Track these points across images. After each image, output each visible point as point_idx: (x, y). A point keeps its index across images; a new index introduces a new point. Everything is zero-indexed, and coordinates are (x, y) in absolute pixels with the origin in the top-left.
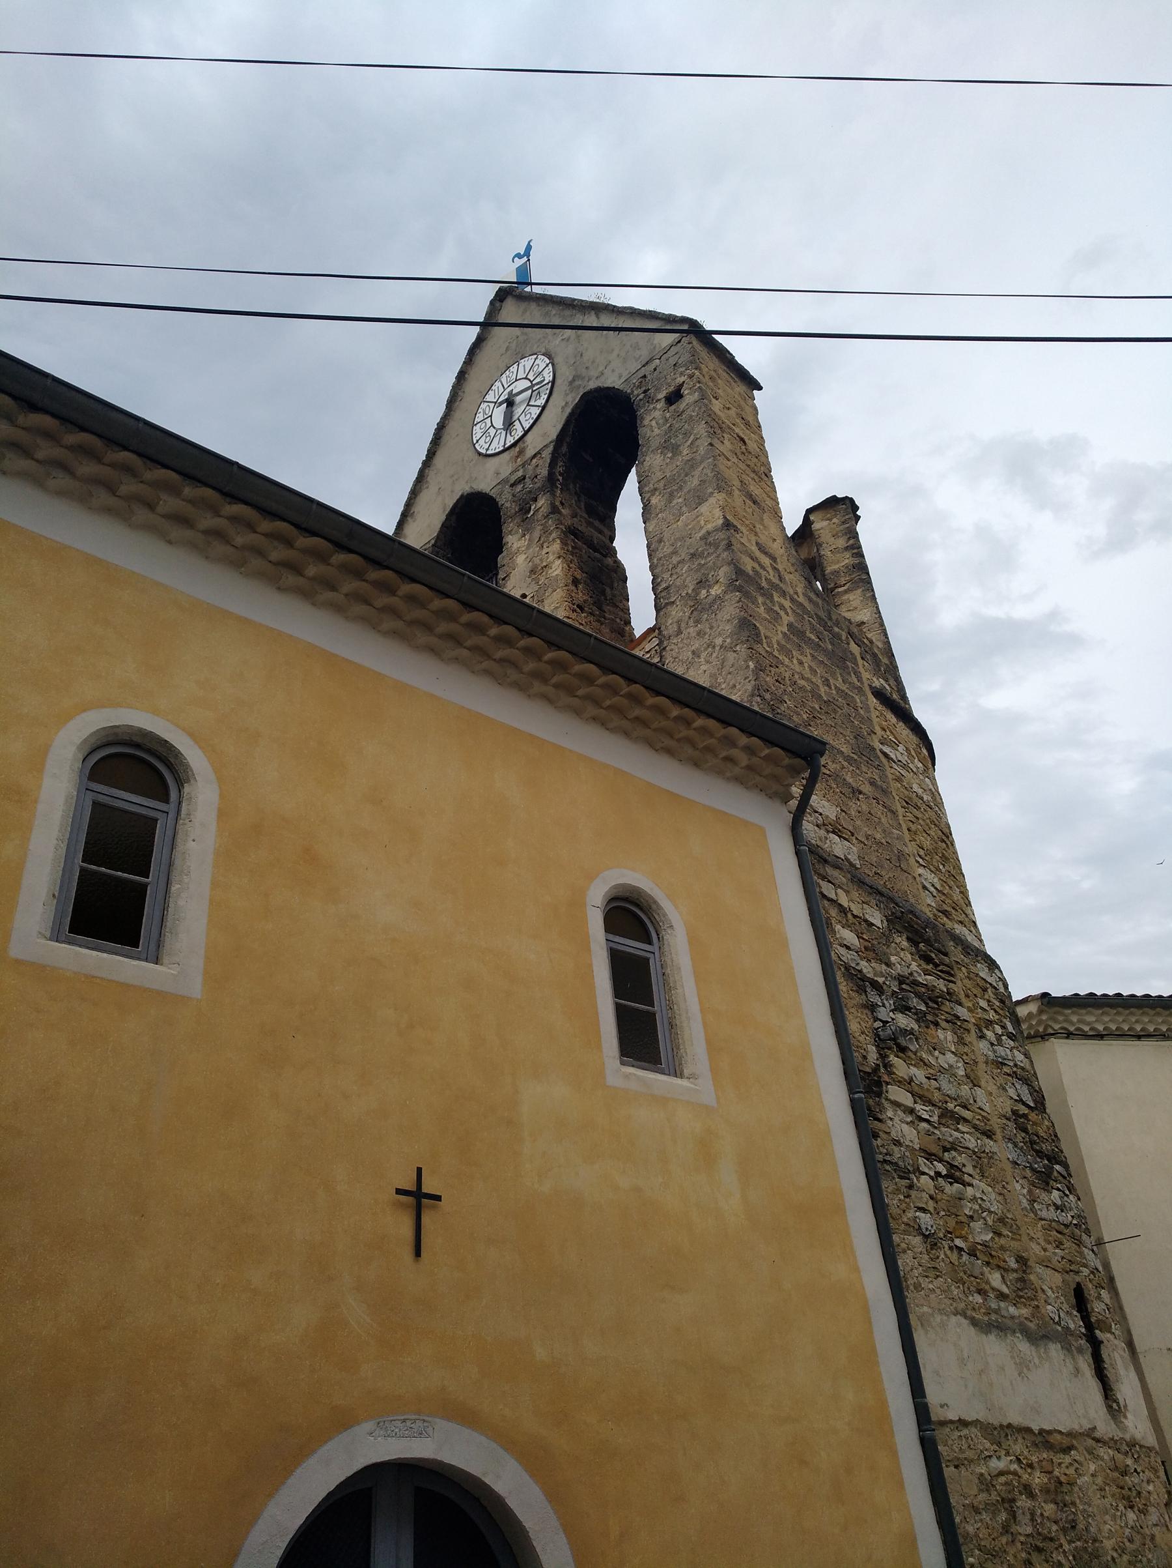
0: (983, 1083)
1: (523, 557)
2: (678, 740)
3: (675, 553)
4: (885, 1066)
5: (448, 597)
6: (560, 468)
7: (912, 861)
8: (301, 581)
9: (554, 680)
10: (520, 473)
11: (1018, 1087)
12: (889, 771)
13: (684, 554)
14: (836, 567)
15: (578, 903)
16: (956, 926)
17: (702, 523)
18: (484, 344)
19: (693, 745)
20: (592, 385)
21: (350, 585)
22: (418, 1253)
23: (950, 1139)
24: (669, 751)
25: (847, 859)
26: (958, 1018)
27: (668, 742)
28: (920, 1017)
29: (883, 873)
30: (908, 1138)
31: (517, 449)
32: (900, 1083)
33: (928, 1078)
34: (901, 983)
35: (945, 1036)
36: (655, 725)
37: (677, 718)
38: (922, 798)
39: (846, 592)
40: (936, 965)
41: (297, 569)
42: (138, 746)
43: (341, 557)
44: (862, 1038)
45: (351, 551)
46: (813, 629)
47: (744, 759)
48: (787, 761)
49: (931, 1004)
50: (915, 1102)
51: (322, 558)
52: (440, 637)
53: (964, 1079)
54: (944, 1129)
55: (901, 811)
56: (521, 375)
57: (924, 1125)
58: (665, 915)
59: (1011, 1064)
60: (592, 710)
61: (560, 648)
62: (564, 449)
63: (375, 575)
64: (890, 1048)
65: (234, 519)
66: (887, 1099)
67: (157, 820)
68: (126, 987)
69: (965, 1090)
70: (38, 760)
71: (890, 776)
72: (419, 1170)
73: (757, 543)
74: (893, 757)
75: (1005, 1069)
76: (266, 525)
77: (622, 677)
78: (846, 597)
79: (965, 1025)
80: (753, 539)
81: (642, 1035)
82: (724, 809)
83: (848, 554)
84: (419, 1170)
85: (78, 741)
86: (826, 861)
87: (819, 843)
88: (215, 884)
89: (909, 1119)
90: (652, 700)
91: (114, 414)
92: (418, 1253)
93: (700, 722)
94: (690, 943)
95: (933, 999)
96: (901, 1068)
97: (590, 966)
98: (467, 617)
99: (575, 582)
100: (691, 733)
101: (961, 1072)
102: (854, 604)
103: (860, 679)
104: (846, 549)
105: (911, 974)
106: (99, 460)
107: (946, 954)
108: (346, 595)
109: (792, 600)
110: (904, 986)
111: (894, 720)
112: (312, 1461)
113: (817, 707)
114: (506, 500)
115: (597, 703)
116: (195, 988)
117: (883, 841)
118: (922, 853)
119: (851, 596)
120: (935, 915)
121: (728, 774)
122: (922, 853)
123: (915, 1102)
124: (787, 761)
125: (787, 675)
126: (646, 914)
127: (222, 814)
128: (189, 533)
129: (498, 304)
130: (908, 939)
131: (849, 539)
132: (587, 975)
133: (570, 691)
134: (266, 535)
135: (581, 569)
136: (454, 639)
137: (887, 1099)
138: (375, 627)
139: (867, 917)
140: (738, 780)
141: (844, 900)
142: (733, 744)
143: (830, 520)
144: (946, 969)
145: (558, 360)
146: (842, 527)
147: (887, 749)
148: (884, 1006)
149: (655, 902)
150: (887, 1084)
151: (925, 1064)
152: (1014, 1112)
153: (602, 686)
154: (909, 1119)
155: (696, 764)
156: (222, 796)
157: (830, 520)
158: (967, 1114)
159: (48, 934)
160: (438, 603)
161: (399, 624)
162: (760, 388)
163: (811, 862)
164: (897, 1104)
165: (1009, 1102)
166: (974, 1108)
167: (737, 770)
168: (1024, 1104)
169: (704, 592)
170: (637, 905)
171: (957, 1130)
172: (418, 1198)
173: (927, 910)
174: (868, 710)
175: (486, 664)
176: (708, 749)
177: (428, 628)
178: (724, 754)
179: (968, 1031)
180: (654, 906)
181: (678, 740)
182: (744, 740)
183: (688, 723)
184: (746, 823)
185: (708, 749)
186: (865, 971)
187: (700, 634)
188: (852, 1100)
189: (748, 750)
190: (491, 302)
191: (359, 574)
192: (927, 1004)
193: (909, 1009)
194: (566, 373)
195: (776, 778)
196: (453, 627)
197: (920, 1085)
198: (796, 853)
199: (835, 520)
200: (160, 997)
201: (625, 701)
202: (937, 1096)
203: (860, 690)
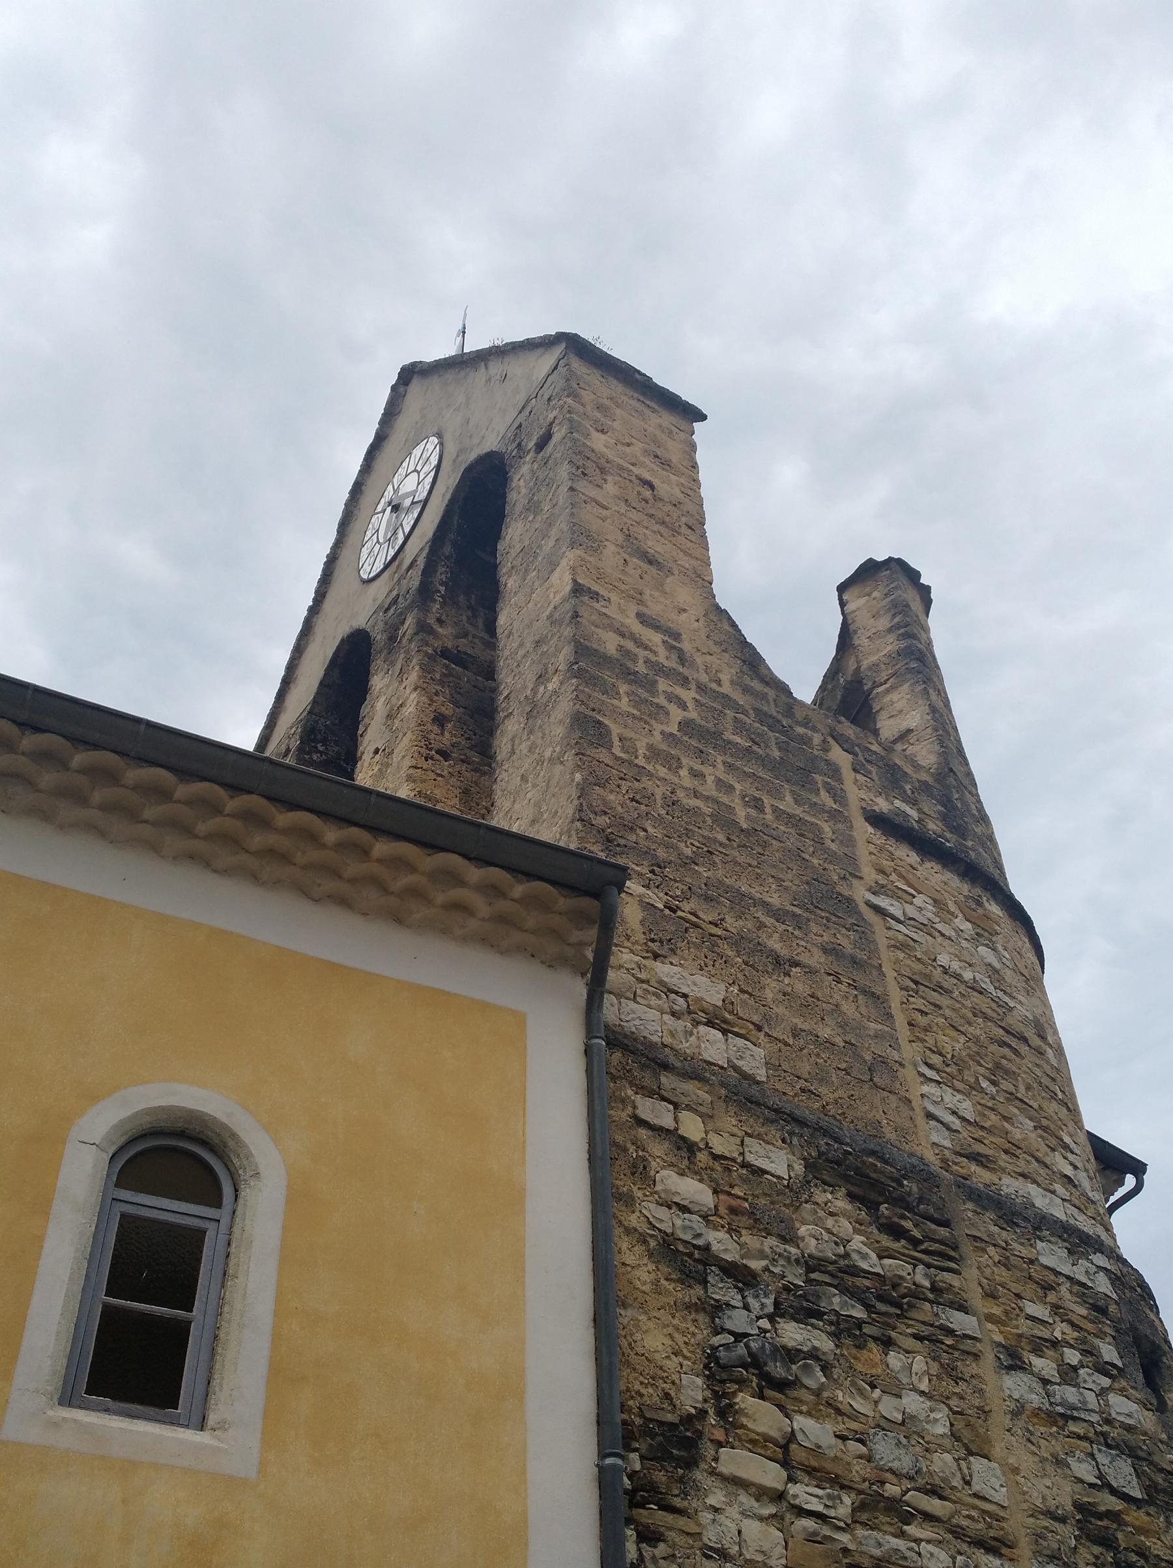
0: (998, 1450)
1: (383, 699)
2: (352, 881)
3: (521, 645)
4: (722, 1413)
6: (442, 574)
7: (908, 1074)
10: (395, 593)
11: (1101, 1459)
12: (881, 937)
13: (529, 645)
14: (874, 659)
16: (1006, 1180)
17: (552, 595)
18: (385, 444)
19: (385, 890)
20: (472, 456)
23: (877, 1552)
24: (343, 902)
25: (736, 1069)
26: (950, 1332)
27: (329, 885)
28: (843, 1329)
29: (823, 1090)
30: (753, 1546)
31: (396, 563)
32: (757, 1444)
33: (843, 1438)
34: (810, 1269)
35: (911, 1364)
37: (340, 846)
38: (958, 977)
39: (888, 691)
40: (915, 1242)
44: (672, 1364)
46: (740, 727)
47: (482, 906)
49: (881, 1307)
50: (791, 1479)
53: (947, 1442)
54: (861, 1532)
55: (896, 997)
56: (411, 468)
57: (809, 1524)
58: (249, 1156)
59: (1095, 1418)
61: (96, 746)
62: (448, 549)
64: (742, 1383)
66: (713, 1472)
69: (943, 1463)
71: (882, 943)
73: (639, 615)
74: (898, 913)
75: (1073, 1427)
78: (887, 699)
79: (968, 1345)
80: (633, 608)
83: (891, 638)
86: (666, 1067)
87: (668, 1040)
89: (770, 1510)
90: (285, 819)
93: (382, 848)
94: (290, 1200)
95: (890, 1299)
96: (760, 1414)
97: (39, 1240)
99: (440, 720)
100: (374, 868)
101: (941, 1429)
102: (898, 706)
103: (839, 796)
104: (890, 630)
105: (847, 1255)
107: (945, 1224)
109: (701, 688)
110: (813, 1276)
111: (914, 858)
113: (721, 837)
114: (379, 637)
115: (187, 831)
117: (839, 1041)
118: (936, 1060)
119: (894, 696)
120: (944, 1161)
122: (936, 1060)
123: (791, 1479)
124: (564, 902)
125: (659, 793)
129: (402, 389)
130: (851, 1196)
131: (894, 616)
135: (456, 703)
137: (713, 1472)
139: (750, 1158)
140: (486, 941)
141: (692, 1128)
143: (869, 595)
144: (935, 1247)
145: (448, 437)
146: (884, 602)
147: (882, 902)
148: (746, 1307)
149: (234, 1136)
150: (720, 1445)
151: (839, 1412)
152: (1079, 1506)
154: (770, 1510)
155: (398, 919)
157: (869, 595)
158: (934, 1505)
162: (703, 417)
163: (619, 1062)
164: (737, 1483)
165: (1068, 1487)
166: (965, 1495)
167: (473, 924)
168: (1114, 1491)
169: (542, 689)
170: (204, 1143)
171: (902, 1535)
173: (930, 1156)
174: (849, 842)
176: (414, 892)
178: (440, 898)
179: (976, 1356)
180: (231, 1144)
182: (475, 874)
184: (484, 1007)
185: (414, 892)
186: (715, 1247)
187: (531, 750)
188: (601, 1469)
189: (494, 891)
190: (393, 388)
192: (868, 1308)
193: (819, 1315)
194: (451, 449)
197: (816, 1451)
198: (587, 1052)
199: (876, 594)
201: (238, 824)
202: (859, 1471)
203: (835, 816)
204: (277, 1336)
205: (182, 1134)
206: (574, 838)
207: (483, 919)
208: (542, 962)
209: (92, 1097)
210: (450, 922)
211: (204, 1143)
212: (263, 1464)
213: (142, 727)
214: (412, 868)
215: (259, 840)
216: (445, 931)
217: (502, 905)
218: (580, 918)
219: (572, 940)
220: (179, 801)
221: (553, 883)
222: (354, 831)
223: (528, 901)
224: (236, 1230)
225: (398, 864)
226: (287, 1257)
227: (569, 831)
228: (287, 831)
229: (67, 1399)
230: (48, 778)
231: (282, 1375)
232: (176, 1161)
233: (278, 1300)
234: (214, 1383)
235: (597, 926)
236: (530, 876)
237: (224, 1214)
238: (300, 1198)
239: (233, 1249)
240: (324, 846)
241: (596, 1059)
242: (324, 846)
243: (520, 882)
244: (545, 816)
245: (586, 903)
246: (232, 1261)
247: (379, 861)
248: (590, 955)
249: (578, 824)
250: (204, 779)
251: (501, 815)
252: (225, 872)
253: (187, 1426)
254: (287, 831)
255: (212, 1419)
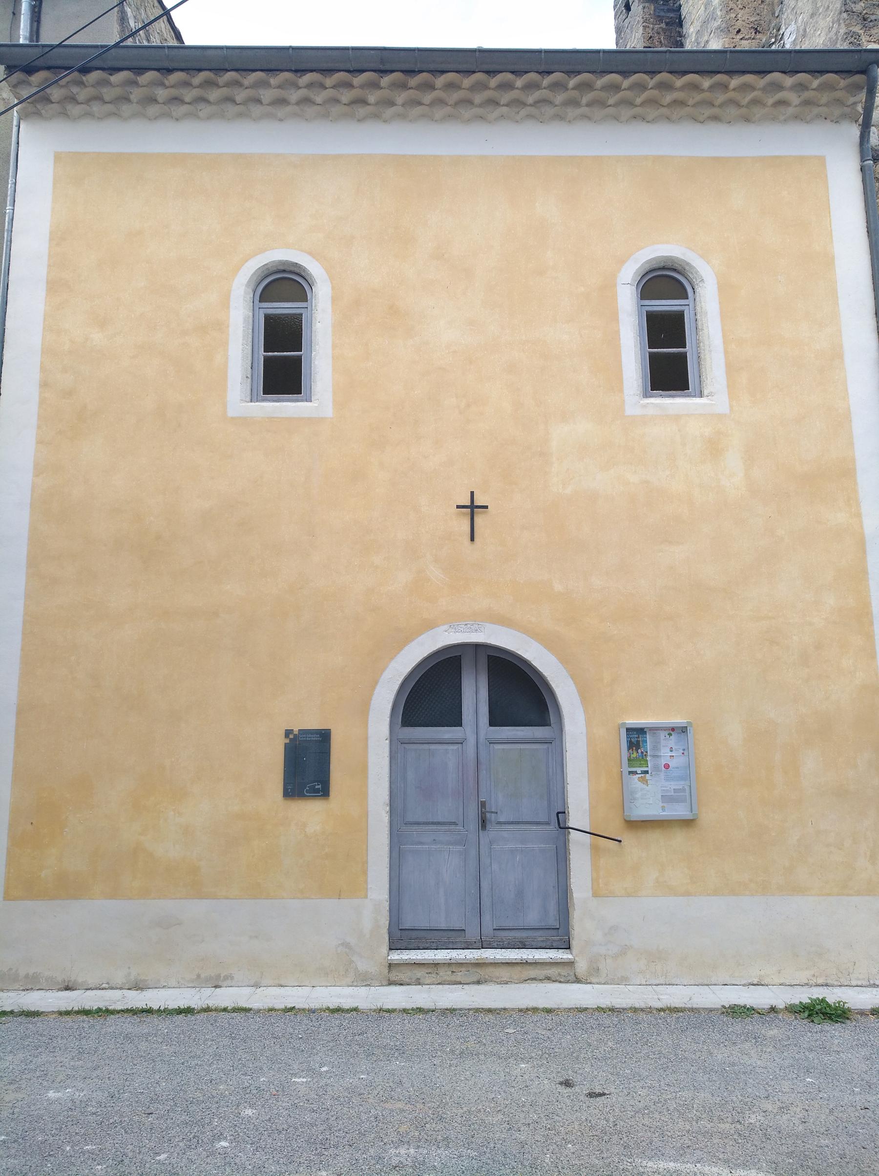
2: (720, 106)
5: (474, 72)
8: (369, 109)
9: (584, 101)
15: (609, 287)
19: (738, 105)
21: (401, 97)
22: (472, 539)
24: (716, 118)
27: (708, 112)
36: (691, 102)
37: (711, 87)
41: (363, 102)
42: (284, 271)
43: (386, 80)
45: (392, 71)
47: (794, 98)
48: (843, 83)
51: (375, 85)
52: (480, 106)
60: (626, 112)
61: (579, 73)
63: (414, 81)
65: (310, 86)
67: (302, 314)
68: (290, 419)
70: (225, 303)
72: (472, 493)
76: (329, 81)
77: (645, 72)
81: (669, 372)
82: (777, 153)
84: (472, 493)
85: (245, 282)
88: (334, 346)
90: (679, 82)
91: (209, 52)
92: (472, 539)
97: (618, 332)
98: (494, 82)
100: (731, 94)
106: (217, 85)
108: (403, 105)
112: (413, 644)
115: (630, 104)
116: (328, 411)
121: (782, 118)
126: (683, 275)
127: (334, 300)
128: (289, 109)
132: (613, 340)
133: (601, 103)
134: (334, 87)
136: (493, 102)
138: (431, 118)
140: (797, 118)
142: (779, 87)
149: (688, 264)
153: (630, 88)
156: (333, 288)
159: (248, 399)
160: (467, 82)
161: (448, 110)
167: (790, 110)
170: (675, 270)
172: (473, 508)
175: (524, 112)
177: (469, 102)
178: (770, 101)
180: (687, 268)
181: (720, 106)
182: (789, 81)
183: (725, 87)
184: (801, 159)
185: (755, 102)
189: (801, 87)
191: (404, 86)
195: (839, 102)
196: (487, 94)
200: (310, 421)
201: (655, 92)
204: (726, 352)
205: (664, 268)
206: (843, 25)
207: (796, 106)
208: (832, 121)
209: (622, 262)
210: (779, 112)
211: (675, 270)
212: (731, 407)
213: (601, 54)
214: (753, 88)
215: (669, 98)
216: (774, 119)
217: (807, 95)
218: (855, 88)
219: (849, 103)
220: (625, 89)
221: (836, 72)
222: (719, 76)
223: (821, 88)
224: (698, 308)
225: (745, 88)
226: (723, 316)
227: (839, 20)
228: (682, 88)
229: (646, 395)
230: (559, 98)
231: (731, 369)
232: (664, 282)
233: (724, 336)
234: (703, 377)
235: (865, 90)
236: (822, 72)
237: (690, 301)
238: (725, 289)
239: (698, 317)
240: (703, 91)
241: (868, 172)
242: (703, 91)
243: (817, 78)
244: (821, 10)
245: (859, 78)
246: (699, 323)
247: (734, 90)
248: (860, 109)
249: (845, 15)
250: (635, 73)
251: (789, 11)
252: (653, 121)
253: (695, 396)
254: (682, 88)
255: (706, 392)
